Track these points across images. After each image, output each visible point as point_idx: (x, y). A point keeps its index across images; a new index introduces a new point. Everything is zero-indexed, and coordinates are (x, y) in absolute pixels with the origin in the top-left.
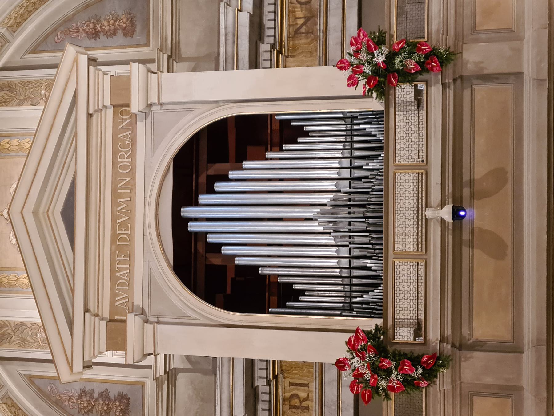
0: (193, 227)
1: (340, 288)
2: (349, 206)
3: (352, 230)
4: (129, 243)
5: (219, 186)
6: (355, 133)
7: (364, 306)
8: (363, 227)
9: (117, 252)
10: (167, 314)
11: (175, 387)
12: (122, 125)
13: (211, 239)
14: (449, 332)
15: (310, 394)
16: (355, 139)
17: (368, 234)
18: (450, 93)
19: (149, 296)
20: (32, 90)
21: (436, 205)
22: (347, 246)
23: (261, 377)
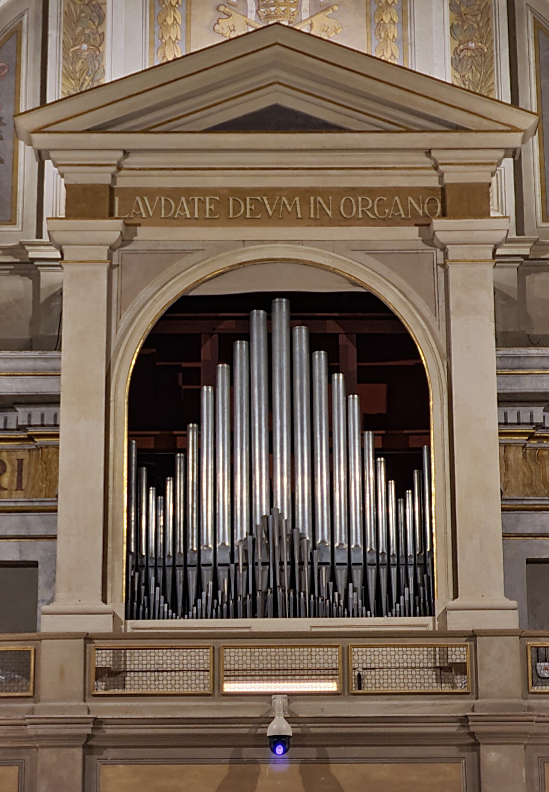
0: (258, 316)
1: (170, 549)
2: (292, 563)
3: (256, 567)
4: (231, 216)
5: (320, 357)
6: (402, 570)
7: (143, 587)
8: (261, 585)
9: (218, 198)
10: (123, 280)
11: (11, 274)
12: (413, 202)
13: (240, 347)
14: (109, 731)
15: (6, 492)
16: (394, 570)
17: (250, 592)
18: (453, 728)
19: (152, 252)
20: (475, 25)
21: (291, 708)
22: (232, 560)
23: (30, 416)
